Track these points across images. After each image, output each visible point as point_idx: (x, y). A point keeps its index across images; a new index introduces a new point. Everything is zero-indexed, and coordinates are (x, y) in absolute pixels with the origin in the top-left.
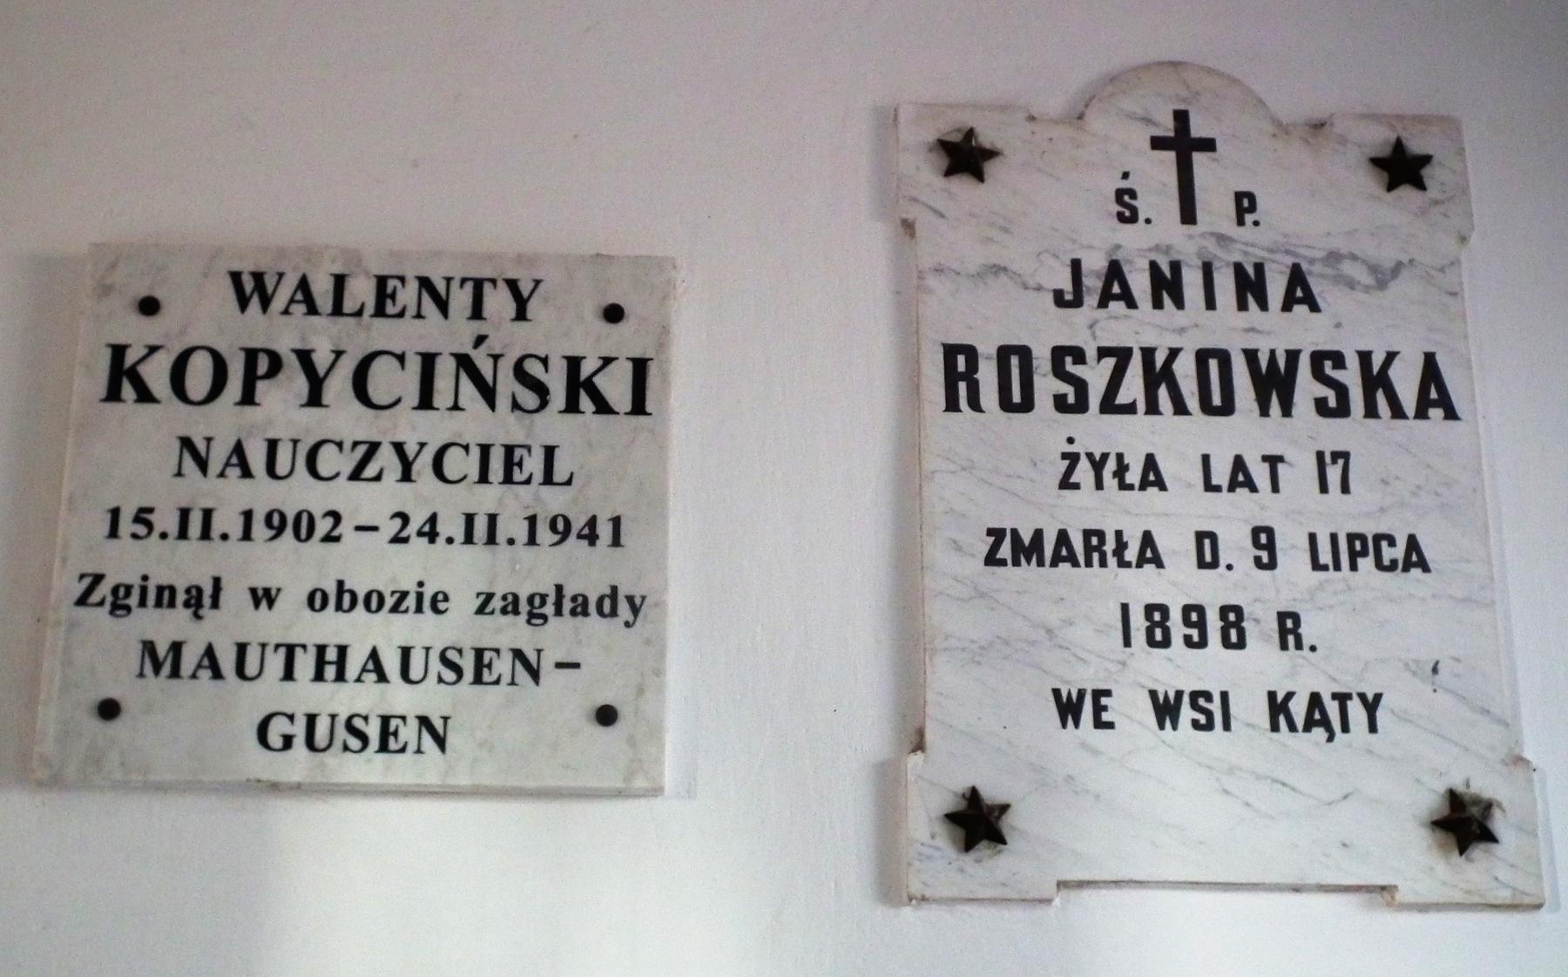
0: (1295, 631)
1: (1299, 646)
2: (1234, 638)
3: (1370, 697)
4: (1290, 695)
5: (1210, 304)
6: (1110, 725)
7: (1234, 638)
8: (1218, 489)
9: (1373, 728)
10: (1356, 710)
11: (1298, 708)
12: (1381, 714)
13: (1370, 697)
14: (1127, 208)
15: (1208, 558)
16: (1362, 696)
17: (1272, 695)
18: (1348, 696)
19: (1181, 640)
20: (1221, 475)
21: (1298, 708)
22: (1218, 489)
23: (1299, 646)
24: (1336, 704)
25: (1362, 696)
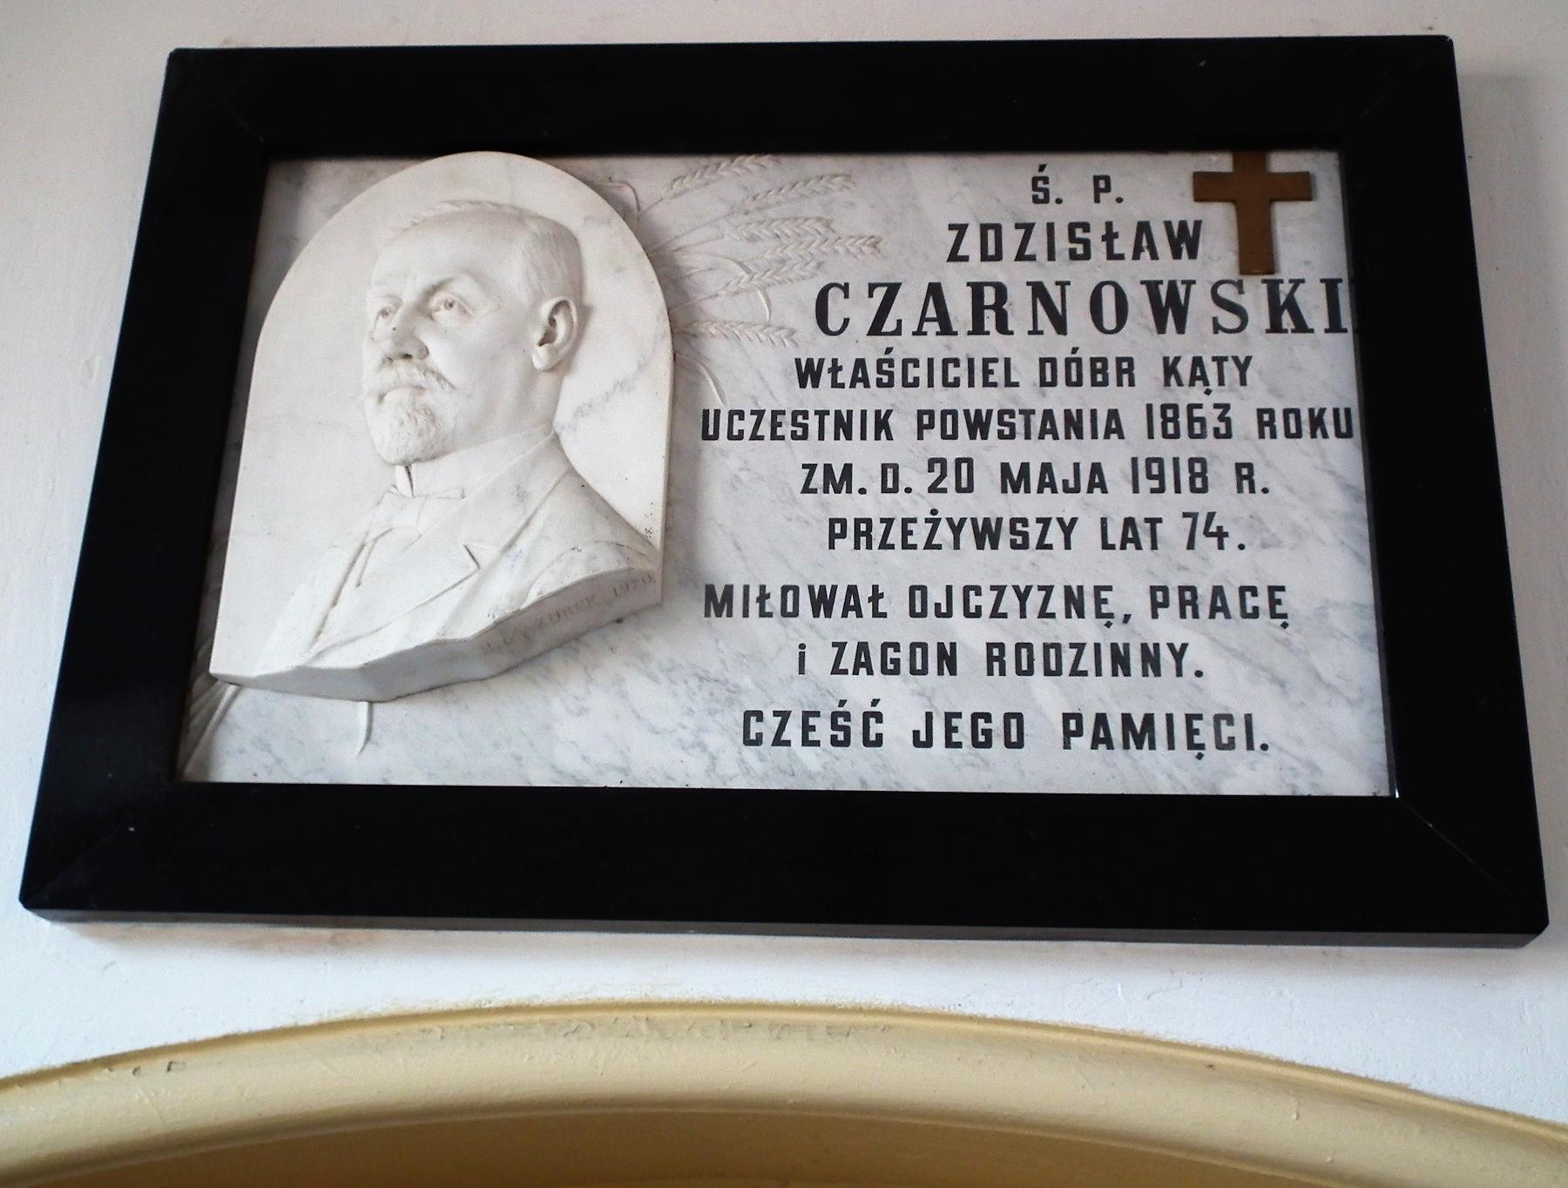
0: (1250, 477)
1: (1252, 490)
2: (1159, 594)
3: (1242, 360)
4: (1177, 359)
5: (1169, 718)
6: (884, 615)
7: (1159, 594)
8: (1112, 547)
9: (1243, 382)
10: (1231, 370)
11: (1184, 369)
12: (1250, 372)
13: (1242, 360)
14: (1245, 474)
15: (1074, 378)
16: (1236, 359)
17: (1166, 359)
18: (1226, 359)
19: (1067, 254)
20: (1115, 537)
21: (1184, 369)
22: (1112, 547)
23: (1252, 490)
24: (1215, 364)
25: (1236, 359)
